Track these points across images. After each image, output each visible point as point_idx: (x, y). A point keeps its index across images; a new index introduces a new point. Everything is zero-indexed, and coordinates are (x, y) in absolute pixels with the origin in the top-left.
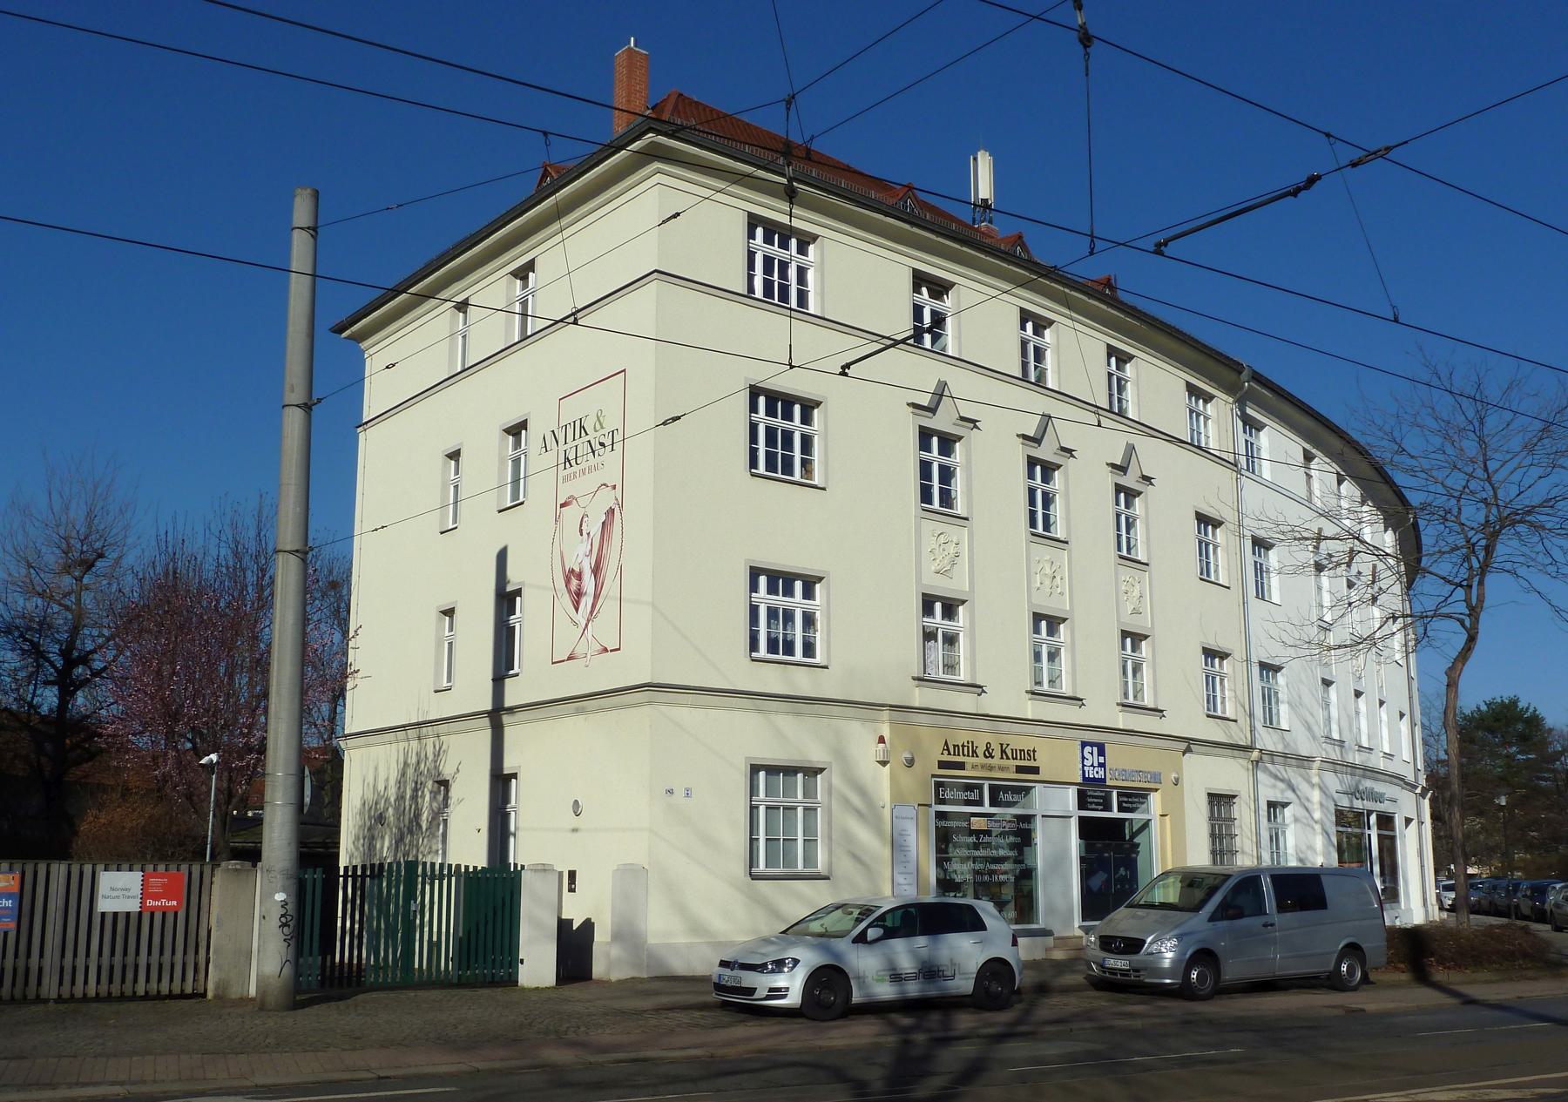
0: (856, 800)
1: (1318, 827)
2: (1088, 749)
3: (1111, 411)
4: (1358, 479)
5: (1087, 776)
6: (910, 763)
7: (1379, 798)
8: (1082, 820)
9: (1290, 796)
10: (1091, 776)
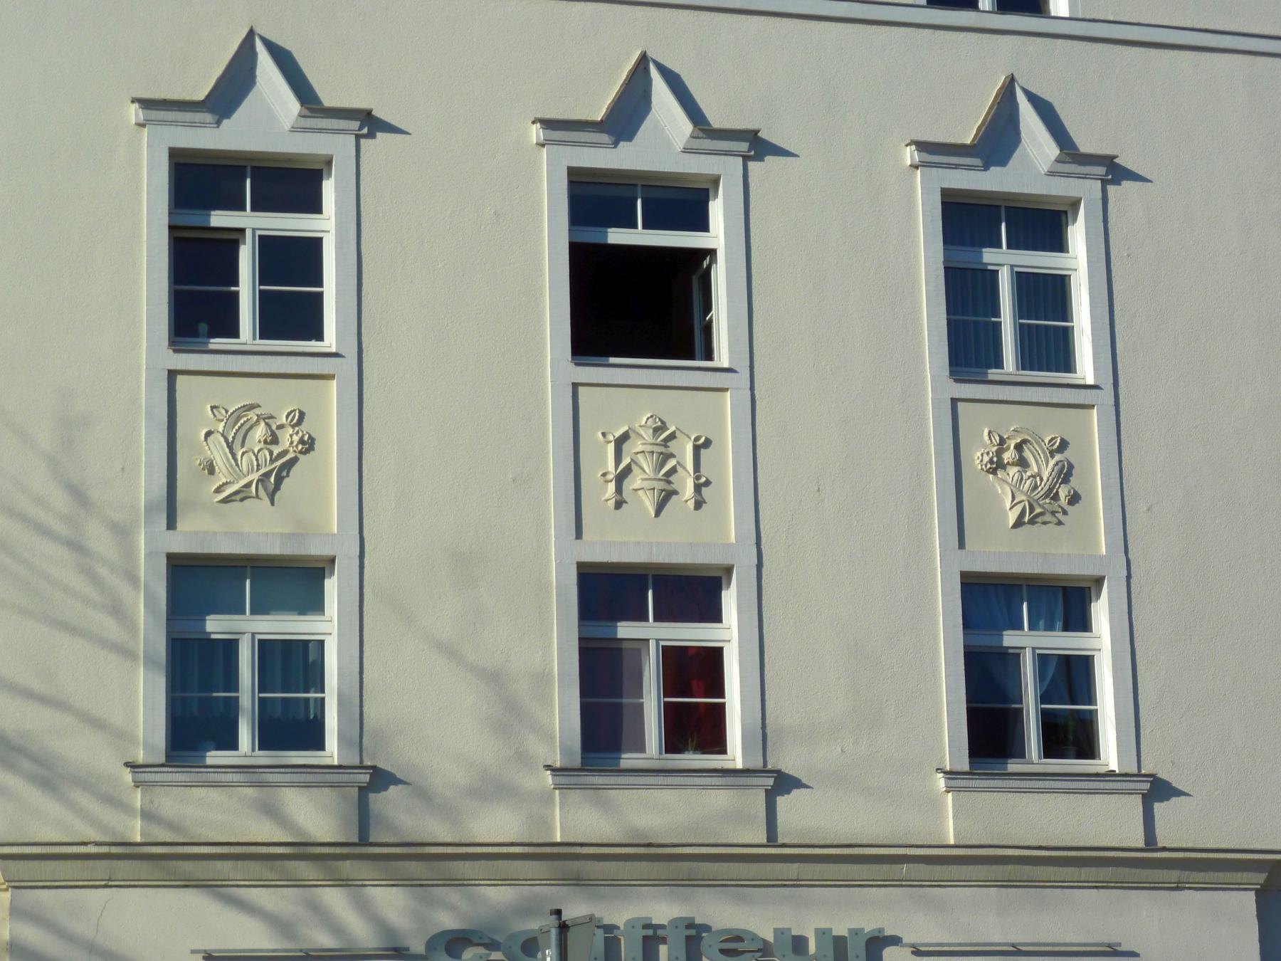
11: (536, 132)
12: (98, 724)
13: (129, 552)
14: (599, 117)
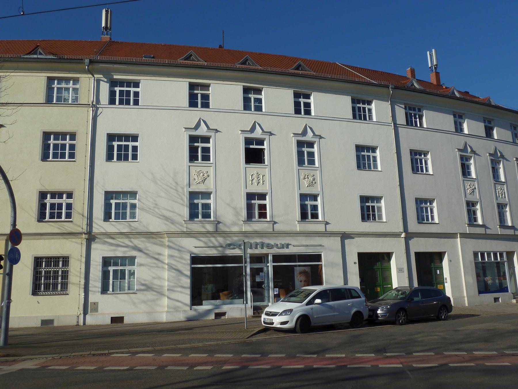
1: (166, 267)
7: (269, 246)
9: (133, 253)
13: (184, 191)
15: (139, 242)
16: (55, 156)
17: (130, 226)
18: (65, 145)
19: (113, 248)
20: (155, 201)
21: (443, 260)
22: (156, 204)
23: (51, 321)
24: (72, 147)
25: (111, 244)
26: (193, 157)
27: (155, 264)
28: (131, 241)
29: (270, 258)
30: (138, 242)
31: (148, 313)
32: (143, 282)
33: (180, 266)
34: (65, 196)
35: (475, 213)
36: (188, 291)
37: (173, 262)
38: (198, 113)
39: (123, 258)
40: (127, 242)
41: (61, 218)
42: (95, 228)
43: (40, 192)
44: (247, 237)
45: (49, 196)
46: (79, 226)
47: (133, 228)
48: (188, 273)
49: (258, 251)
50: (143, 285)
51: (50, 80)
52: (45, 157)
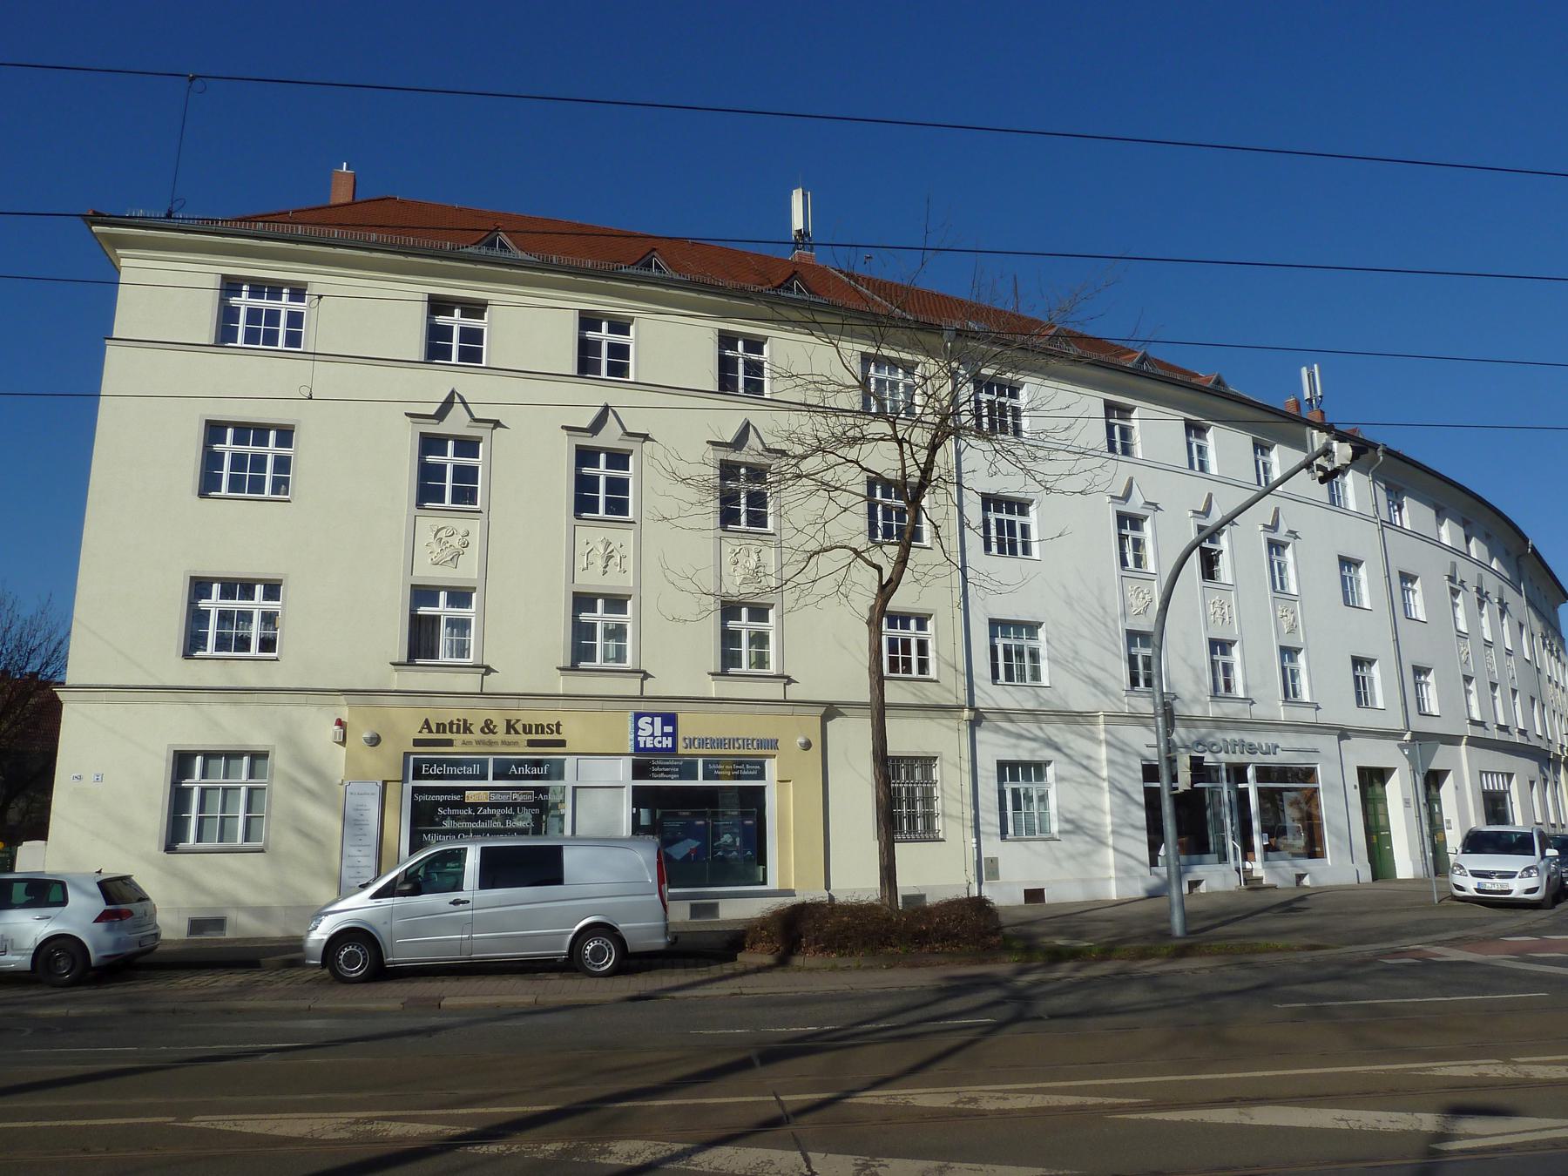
0: (309, 782)
1: (1106, 785)
2: (643, 722)
3: (1391, 523)
4: (1486, 538)
5: (642, 745)
6: (375, 741)
7: (1252, 750)
8: (635, 789)
9: (1046, 754)
10: (649, 745)
11: (1190, 514)
12: (1115, 678)
13: (1117, 627)
14: (433, 413)
15: (1055, 732)
16: (236, 484)
17: (1037, 695)
18: (263, 458)
19: (1013, 741)
20: (1074, 644)
21: (1443, 782)
22: (1076, 653)
23: (219, 923)
24: (283, 464)
25: (1009, 733)
26: (428, 489)
27: (1084, 777)
28: (1041, 729)
29: (1250, 772)
30: (1054, 731)
31: (1084, 881)
32: (1069, 816)
33: (1126, 783)
34: (259, 589)
35: (1294, 675)
36: (1146, 832)
37: (1116, 776)
38: (593, 395)
39: (1026, 765)
40: (1034, 729)
41: (248, 649)
42: (979, 697)
43: (192, 578)
44: (1218, 728)
45: (216, 588)
46: (950, 691)
47: (1042, 701)
48: (1141, 799)
49: (1236, 758)
50: (1068, 821)
51: (230, 286)
52: (208, 485)
